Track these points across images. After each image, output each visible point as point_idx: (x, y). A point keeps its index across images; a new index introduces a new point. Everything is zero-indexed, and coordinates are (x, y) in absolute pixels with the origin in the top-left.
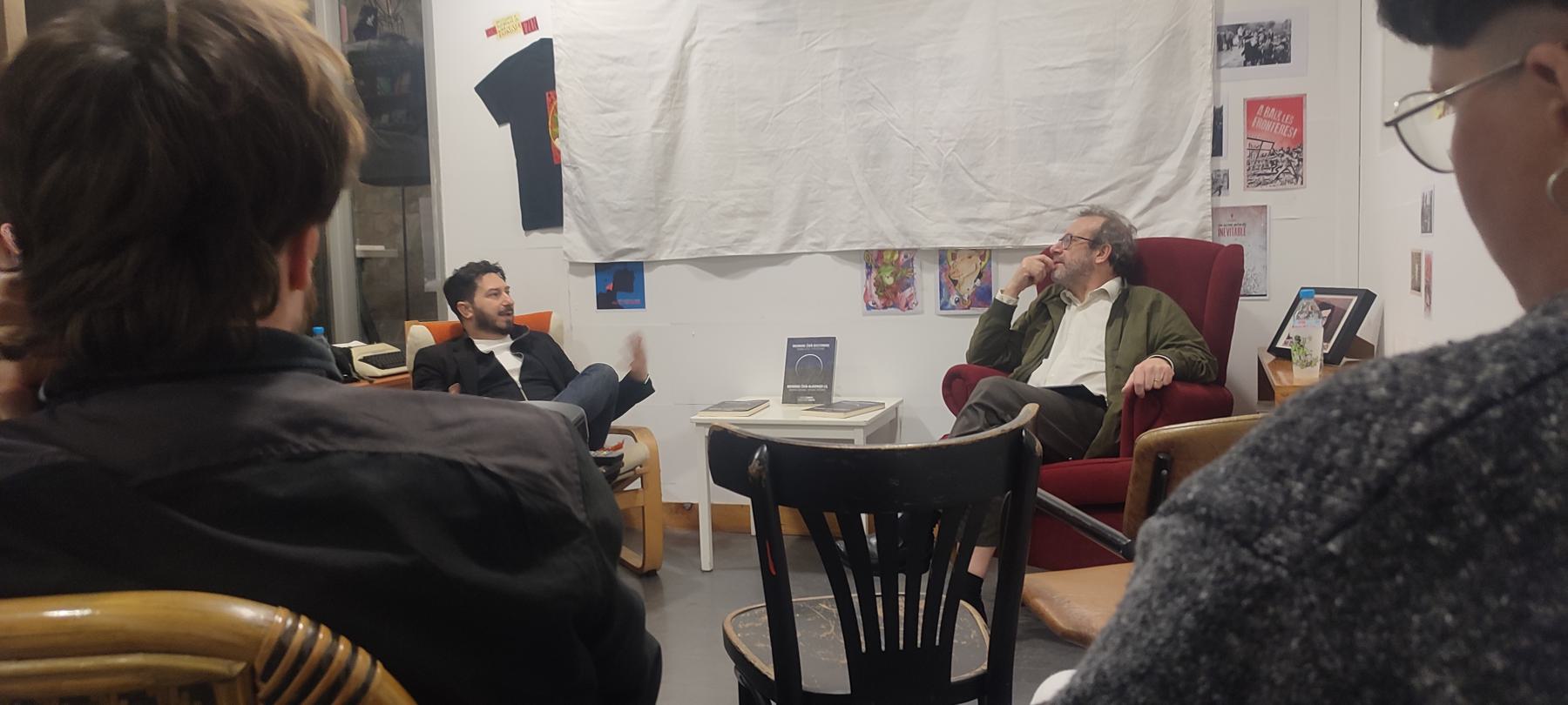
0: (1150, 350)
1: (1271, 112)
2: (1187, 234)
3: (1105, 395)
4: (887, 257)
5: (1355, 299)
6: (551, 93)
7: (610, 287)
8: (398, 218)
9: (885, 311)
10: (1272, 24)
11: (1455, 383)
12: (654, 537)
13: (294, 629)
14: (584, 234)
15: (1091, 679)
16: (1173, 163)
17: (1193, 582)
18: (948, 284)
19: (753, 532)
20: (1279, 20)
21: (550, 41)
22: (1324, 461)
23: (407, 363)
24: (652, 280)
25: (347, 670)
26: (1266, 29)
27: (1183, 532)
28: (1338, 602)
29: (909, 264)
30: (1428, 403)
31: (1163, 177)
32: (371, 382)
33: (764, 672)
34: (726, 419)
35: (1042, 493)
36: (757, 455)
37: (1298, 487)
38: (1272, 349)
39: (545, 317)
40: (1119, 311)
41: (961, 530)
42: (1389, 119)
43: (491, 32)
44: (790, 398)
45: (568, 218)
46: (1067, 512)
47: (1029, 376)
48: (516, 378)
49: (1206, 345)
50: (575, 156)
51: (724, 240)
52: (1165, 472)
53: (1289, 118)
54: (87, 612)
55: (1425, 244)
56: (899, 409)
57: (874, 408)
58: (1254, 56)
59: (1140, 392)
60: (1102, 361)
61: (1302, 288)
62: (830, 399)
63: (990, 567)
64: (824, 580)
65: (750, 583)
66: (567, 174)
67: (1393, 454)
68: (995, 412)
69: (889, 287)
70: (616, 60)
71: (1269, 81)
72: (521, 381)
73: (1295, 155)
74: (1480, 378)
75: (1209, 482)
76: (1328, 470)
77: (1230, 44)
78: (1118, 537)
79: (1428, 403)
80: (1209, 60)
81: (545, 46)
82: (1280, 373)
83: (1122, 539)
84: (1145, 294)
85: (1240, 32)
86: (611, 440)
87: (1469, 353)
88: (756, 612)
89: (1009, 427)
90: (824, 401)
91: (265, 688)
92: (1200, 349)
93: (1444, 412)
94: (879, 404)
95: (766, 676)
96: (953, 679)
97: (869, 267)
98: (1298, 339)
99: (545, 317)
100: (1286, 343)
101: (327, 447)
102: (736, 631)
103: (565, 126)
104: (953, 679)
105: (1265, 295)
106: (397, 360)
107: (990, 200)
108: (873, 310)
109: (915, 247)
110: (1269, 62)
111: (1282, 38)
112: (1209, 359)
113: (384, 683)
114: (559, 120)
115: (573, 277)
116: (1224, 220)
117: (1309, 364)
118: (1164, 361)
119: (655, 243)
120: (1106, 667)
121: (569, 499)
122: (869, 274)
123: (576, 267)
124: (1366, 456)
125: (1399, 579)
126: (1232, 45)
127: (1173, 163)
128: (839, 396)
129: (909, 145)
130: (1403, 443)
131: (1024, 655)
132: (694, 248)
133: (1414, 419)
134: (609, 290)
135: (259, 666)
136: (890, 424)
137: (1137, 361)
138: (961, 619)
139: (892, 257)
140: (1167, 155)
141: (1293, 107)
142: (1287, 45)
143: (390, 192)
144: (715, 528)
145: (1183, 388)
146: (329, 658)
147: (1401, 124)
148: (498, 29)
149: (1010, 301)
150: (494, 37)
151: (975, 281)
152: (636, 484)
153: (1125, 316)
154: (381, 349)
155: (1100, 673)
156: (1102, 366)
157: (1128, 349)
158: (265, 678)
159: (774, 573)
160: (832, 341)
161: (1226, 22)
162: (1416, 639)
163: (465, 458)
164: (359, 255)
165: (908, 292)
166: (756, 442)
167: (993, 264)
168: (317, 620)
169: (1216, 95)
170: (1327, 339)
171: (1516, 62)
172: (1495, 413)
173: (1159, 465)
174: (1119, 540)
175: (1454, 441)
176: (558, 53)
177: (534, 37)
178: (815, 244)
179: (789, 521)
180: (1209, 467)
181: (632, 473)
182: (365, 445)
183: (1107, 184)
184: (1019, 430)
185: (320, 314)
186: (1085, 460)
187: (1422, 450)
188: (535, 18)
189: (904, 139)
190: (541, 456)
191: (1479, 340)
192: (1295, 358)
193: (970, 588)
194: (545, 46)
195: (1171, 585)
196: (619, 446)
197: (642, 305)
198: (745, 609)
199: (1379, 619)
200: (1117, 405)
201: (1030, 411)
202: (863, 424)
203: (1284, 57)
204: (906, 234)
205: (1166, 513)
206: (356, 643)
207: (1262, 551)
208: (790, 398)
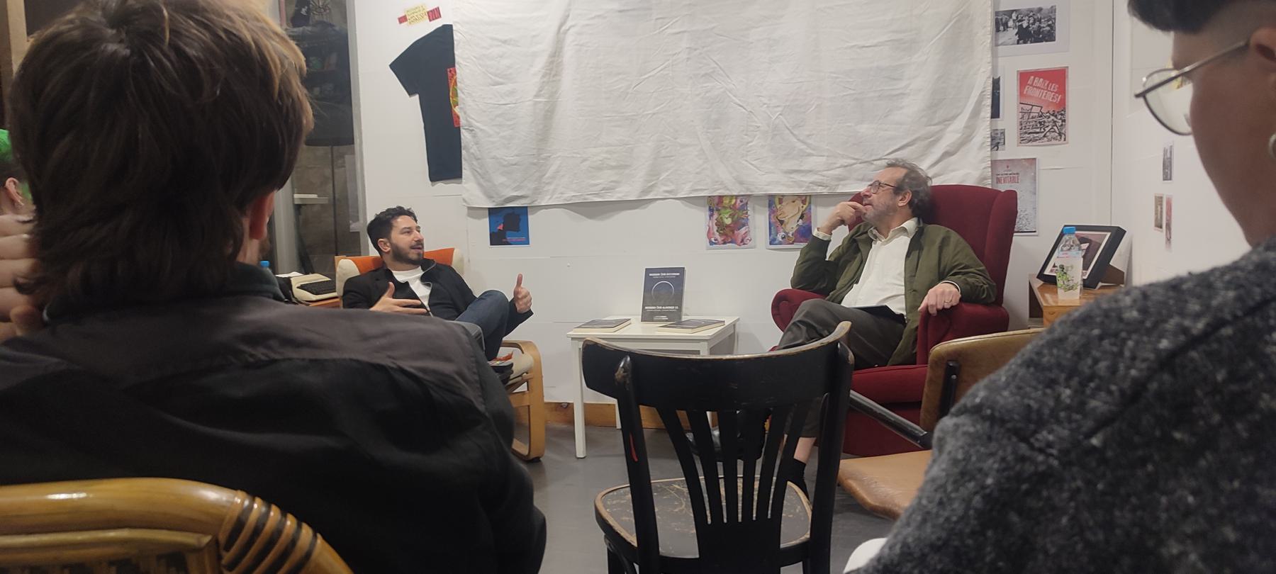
0: (941, 277)
1: (1039, 82)
3: (904, 313)
4: (726, 201)
7: (501, 227)
8: (328, 172)
10: (1040, 10)
11: (1194, 306)
12: (538, 429)
13: (250, 508)
14: (480, 184)
15: (897, 549)
16: (959, 124)
17: (980, 470)
18: (776, 223)
19: (619, 426)
22: (1087, 371)
23: (337, 289)
25: (293, 542)
26: (1035, 14)
27: (972, 430)
28: (1100, 486)
29: (744, 207)
30: (1171, 324)
31: (951, 136)
33: (629, 540)
34: (595, 334)
35: (854, 394)
37: (1066, 393)
38: (1041, 276)
40: (916, 245)
43: (403, 20)
44: (647, 317)
45: (466, 172)
46: (874, 409)
52: (954, 377)
53: (1054, 87)
54: (82, 495)
55: (1165, 189)
58: (1025, 36)
59: (933, 311)
61: (1065, 226)
62: (680, 318)
63: (810, 455)
64: (676, 465)
66: (465, 136)
67: (1144, 366)
69: (728, 226)
70: (505, 42)
71: (1038, 57)
73: (1059, 117)
74: (1214, 303)
75: (994, 389)
77: (1006, 26)
78: (916, 429)
79: (1171, 324)
81: (447, 31)
82: (1048, 296)
83: (920, 431)
84: (937, 232)
86: (503, 352)
87: (1205, 282)
90: (675, 319)
91: (227, 557)
92: (981, 275)
93: (1185, 331)
94: (722, 321)
97: (711, 210)
98: (1062, 267)
100: (1052, 271)
102: (606, 507)
104: (782, 546)
106: (330, 287)
107: (810, 155)
113: (324, 553)
116: (1001, 170)
117: (1071, 288)
119: (537, 191)
120: (910, 540)
122: (711, 216)
123: (473, 211)
124: (1122, 367)
125: (1150, 468)
127: (959, 124)
129: (744, 110)
130: (1152, 356)
131: (840, 525)
132: (570, 195)
133: (1161, 337)
135: (222, 538)
136: (729, 338)
140: (954, 117)
141: (1057, 78)
142: (1052, 27)
144: (588, 423)
145: (969, 308)
146: (278, 532)
147: (1149, 96)
152: (523, 388)
153: (921, 249)
155: (905, 545)
156: (902, 290)
158: (227, 548)
159: (636, 460)
160: (682, 270)
162: (1164, 516)
165: (743, 230)
166: (621, 354)
167: (813, 207)
168: (269, 500)
169: (995, 68)
170: (1085, 267)
171: (1242, 43)
172: (1227, 331)
173: (950, 371)
174: (917, 432)
175: (1194, 354)
177: (437, 24)
179: (648, 417)
180: (993, 376)
181: (520, 378)
184: (836, 342)
185: (269, 253)
187: (1167, 362)
191: (1213, 271)
192: (1060, 283)
193: (795, 472)
194: (447, 31)
196: (509, 357)
199: (1134, 500)
200: (914, 322)
201: (844, 327)
203: (1049, 36)
204: (741, 183)
205: (960, 413)
206: (301, 519)
207: (1037, 445)
208: (647, 317)
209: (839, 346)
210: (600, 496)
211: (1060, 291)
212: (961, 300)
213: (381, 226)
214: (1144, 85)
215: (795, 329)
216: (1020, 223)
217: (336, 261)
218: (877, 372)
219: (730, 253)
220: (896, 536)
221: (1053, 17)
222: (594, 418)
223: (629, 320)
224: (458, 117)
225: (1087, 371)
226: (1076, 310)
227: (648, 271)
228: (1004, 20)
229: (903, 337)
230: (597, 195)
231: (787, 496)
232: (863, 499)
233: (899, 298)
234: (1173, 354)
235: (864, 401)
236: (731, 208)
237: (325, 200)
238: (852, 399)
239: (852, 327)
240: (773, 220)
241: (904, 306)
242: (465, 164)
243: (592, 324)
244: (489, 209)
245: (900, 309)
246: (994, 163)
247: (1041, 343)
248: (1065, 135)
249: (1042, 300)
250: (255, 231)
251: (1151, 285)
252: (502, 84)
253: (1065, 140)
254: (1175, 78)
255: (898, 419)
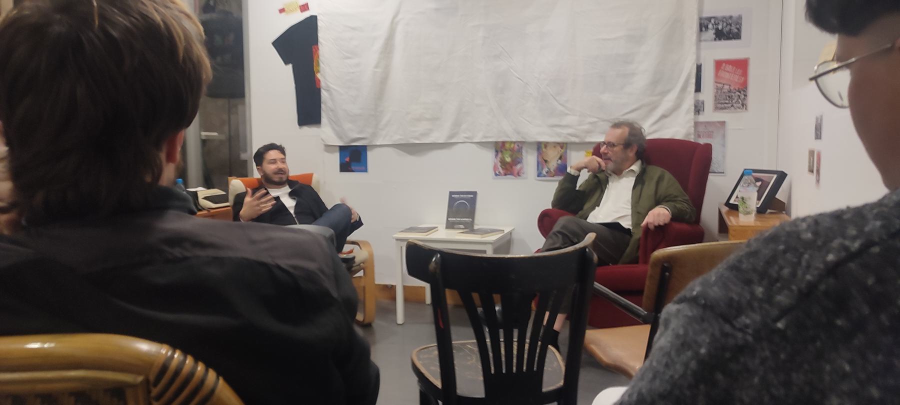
0: (657, 203)
1: (729, 68)
2: (679, 136)
3: (631, 228)
4: (507, 146)
5: (775, 176)
6: (315, 47)
7: (347, 159)
8: (225, 117)
9: (505, 177)
10: (731, 17)
11: (852, 231)
12: (370, 304)
13: (172, 357)
14: (333, 129)
15: (635, 397)
16: (672, 97)
17: (696, 342)
18: (542, 162)
19: (428, 300)
20: (735, 14)
21: (316, 17)
22: (775, 275)
23: (229, 200)
24: (372, 157)
25: (202, 382)
26: (728, 20)
27: (690, 314)
28: (782, 356)
29: (520, 150)
30: (836, 243)
31: (667, 103)
32: (209, 211)
33: (435, 384)
34: (414, 237)
35: (597, 285)
36: (434, 259)
37: (759, 290)
38: (727, 204)
39: (310, 176)
40: (640, 180)
41: (551, 303)
42: (813, 75)
43: (282, 11)
44: (450, 226)
45: (324, 119)
46: (610, 295)
47: (588, 216)
48: (292, 211)
49: (690, 201)
50: (328, 83)
51: (415, 134)
52: (667, 274)
53: (739, 71)
54: (52, 345)
55: (817, 145)
56: (513, 234)
57: (497, 233)
58: (720, 35)
59: (651, 227)
60: (629, 209)
61: (745, 169)
62: (473, 226)
63: (563, 326)
64: (470, 331)
65: (427, 333)
66: (324, 94)
67: (816, 272)
68: (567, 235)
69: (508, 163)
70: (354, 29)
71: (728, 50)
72: (295, 213)
73: (742, 92)
74: (867, 229)
75: (705, 284)
76: (777, 280)
77: (707, 28)
78: (640, 310)
79: (836, 243)
80: (694, 37)
81: (313, 20)
82: (731, 218)
83: (642, 312)
84: (656, 171)
85: (713, 21)
86: (347, 248)
87: (859, 214)
88: (430, 349)
89: (579, 247)
90: (470, 228)
91: (155, 391)
92: (686, 203)
93: (846, 248)
94: (502, 230)
95: (436, 386)
96: (544, 390)
97: (497, 152)
98: (743, 198)
99: (310, 176)
100: (735, 201)
101: (187, 254)
102: (419, 359)
103: (323, 66)
104: (544, 390)
105: (723, 173)
106: (224, 199)
107: (567, 114)
108: (499, 176)
109: (524, 140)
110: (729, 38)
111: (737, 24)
112: (691, 209)
113: (224, 390)
114: (320, 62)
115: (327, 154)
116: (701, 129)
117: (748, 213)
118: (666, 210)
119: (375, 135)
120: (644, 391)
121: (329, 285)
122: (496, 156)
123: (328, 148)
124: (800, 273)
125: (818, 344)
126: (708, 28)
127: (672, 97)
128: (478, 225)
129: (521, 82)
130: (822, 266)
131: (585, 377)
132: (397, 138)
133: (828, 252)
134: (347, 162)
135: (152, 378)
136: (507, 242)
137: (650, 209)
138: (548, 355)
139: (510, 146)
140: (669, 91)
141: (742, 65)
142: (739, 30)
143: (221, 102)
144: (406, 300)
145: (677, 226)
146: (192, 374)
147: (819, 80)
148: (286, 9)
149: (575, 173)
150: (283, 14)
151: (558, 161)
152: (361, 273)
153: (643, 183)
154: (214, 192)
155: (640, 394)
156: (629, 212)
157: (645, 202)
158: (155, 385)
159: (442, 327)
160: (475, 193)
161: (706, 14)
162: (827, 378)
163: (268, 260)
164: (204, 138)
165: (519, 166)
166: (433, 252)
167: (568, 151)
168: (186, 352)
169: (698, 57)
170: (759, 199)
171: (889, 46)
172: (876, 250)
173: (664, 269)
174: (640, 312)
175: (852, 265)
176: (320, 24)
177: (307, 14)
178: (466, 138)
179: (451, 297)
180: (705, 276)
181: (358, 267)
182: (211, 253)
183: (634, 107)
184: (584, 248)
185: (182, 173)
186: (619, 265)
187: (833, 270)
188: (307, 4)
189: (519, 78)
190: (312, 259)
191: (865, 206)
192: (741, 209)
193: (552, 338)
194: (313, 20)
195: (683, 344)
196: (351, 252)
197: (366, 170)
198: (426, 346)
199: (806, 366)
200: (638, 234)
201: (590, 237)
202: (492, 242)
203: (737, 36)
204: (518, 133)
205: (680, 301)
206: (208, 365)
207: (738, 326)
208: (450, 226)
209: (587, 250)
210: (415, 352)
211: (741, 215)
212: (672, 219)
213: (259, 157)
214: (816, 72)
215: (554, 237)
216: (714, 166)
217: (229, 180)
218: (611, 268)
219: (509, 182)
220: (633, 387)
221: (739, 22)
222: (412, 298)
223: (437, 227)
224: (319, 81)
225: (775, 275)
226: (767, 231)
227: (451, 193)
228: (705, 23)
229: (630, 245)
230: (417, 138)
231: (548, 355)
232: (601, 359)
233: (628, 217)
234: (838, 264)
235: (602, 289)
236: (510, 150)
237: (223, 137)
238: (595, 288)
239: (596, 238)
240: (540, 160)
241: (630, 223)
242: (323, 114)
243: (411, 230)
244: (340, 147)
245: (628, 225)
246: (696, 124)
247: (741, 254)
248: (746, 106)
249: (727, 220)
250: (170, 158)
251: (821, 215)
252: (349, 58)
253: (746, 108)
254: (834, 70)
255: (626, 302)
